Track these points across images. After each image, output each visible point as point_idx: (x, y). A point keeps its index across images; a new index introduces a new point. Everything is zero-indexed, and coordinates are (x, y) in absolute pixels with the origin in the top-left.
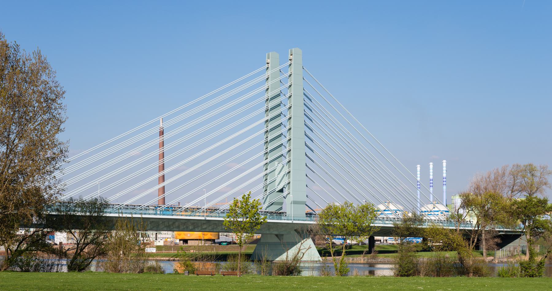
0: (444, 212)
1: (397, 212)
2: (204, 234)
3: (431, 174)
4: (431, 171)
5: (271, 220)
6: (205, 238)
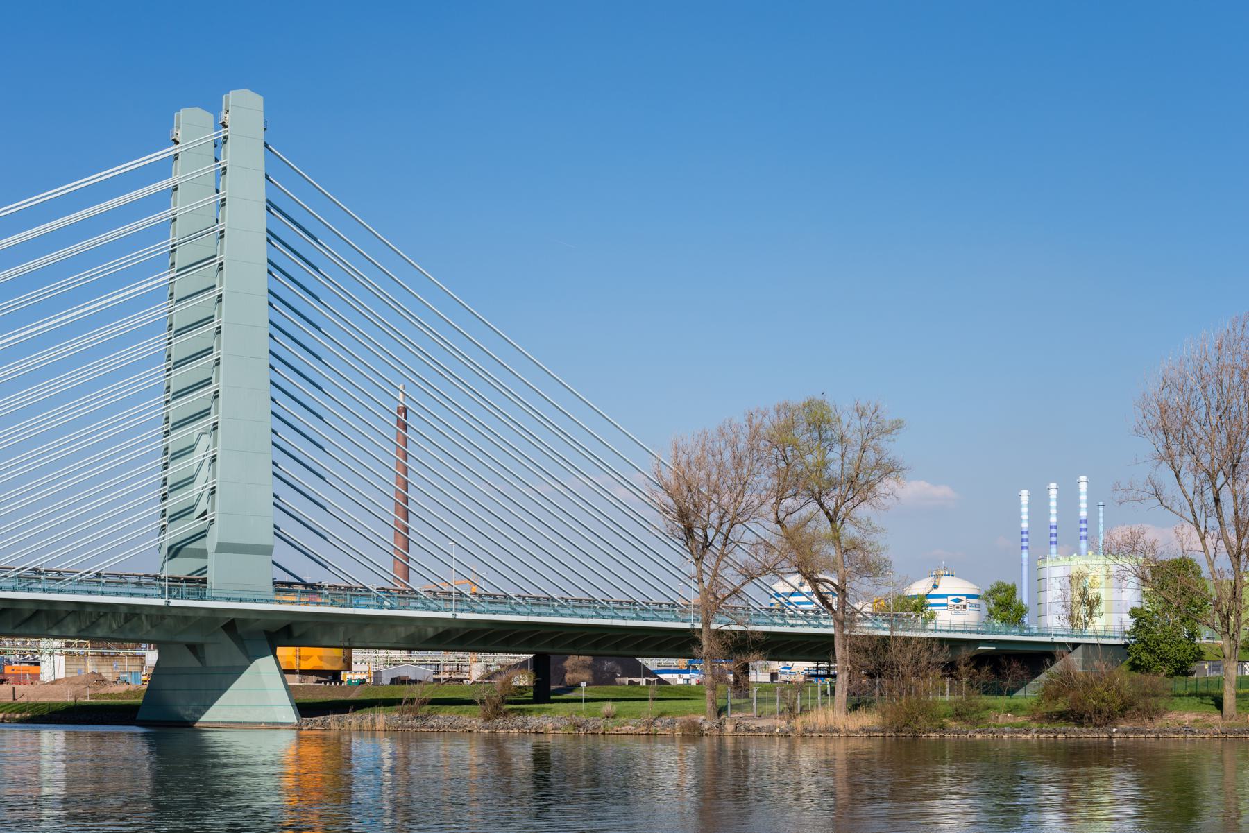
0: (963, 598)
1: (962, 601)
2: (300, 657)
3: (1053, 511)
4: (1053, 504)
5: (980, 635)
6: (303, 667)
